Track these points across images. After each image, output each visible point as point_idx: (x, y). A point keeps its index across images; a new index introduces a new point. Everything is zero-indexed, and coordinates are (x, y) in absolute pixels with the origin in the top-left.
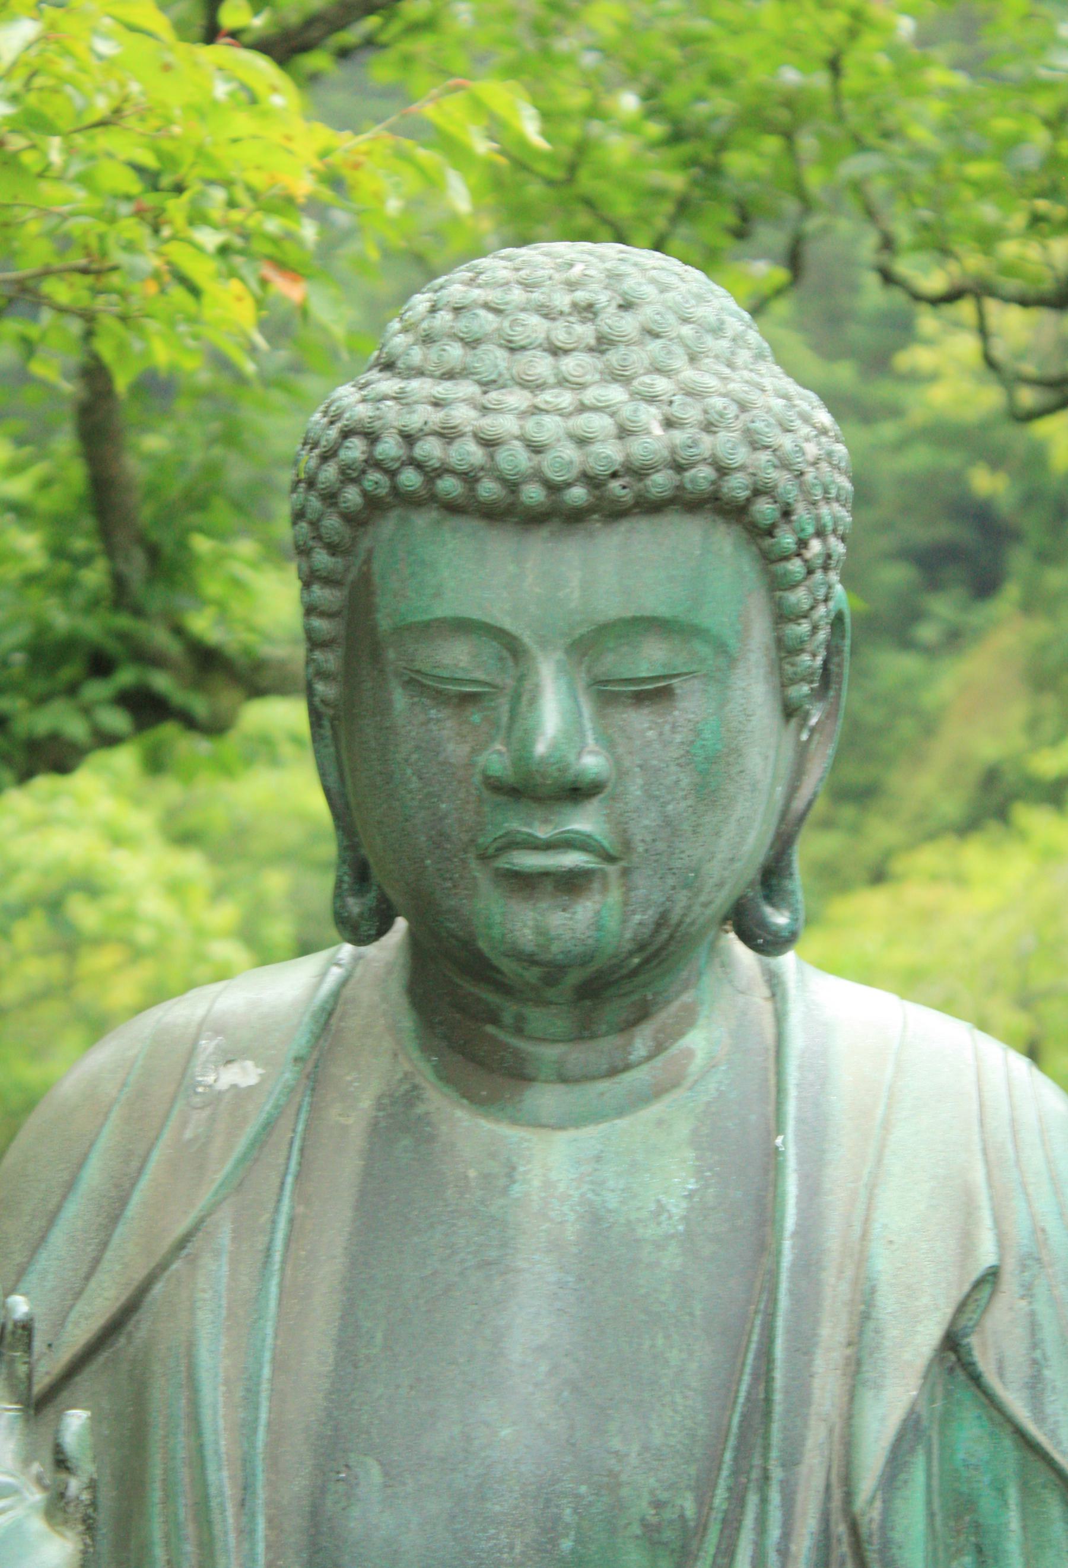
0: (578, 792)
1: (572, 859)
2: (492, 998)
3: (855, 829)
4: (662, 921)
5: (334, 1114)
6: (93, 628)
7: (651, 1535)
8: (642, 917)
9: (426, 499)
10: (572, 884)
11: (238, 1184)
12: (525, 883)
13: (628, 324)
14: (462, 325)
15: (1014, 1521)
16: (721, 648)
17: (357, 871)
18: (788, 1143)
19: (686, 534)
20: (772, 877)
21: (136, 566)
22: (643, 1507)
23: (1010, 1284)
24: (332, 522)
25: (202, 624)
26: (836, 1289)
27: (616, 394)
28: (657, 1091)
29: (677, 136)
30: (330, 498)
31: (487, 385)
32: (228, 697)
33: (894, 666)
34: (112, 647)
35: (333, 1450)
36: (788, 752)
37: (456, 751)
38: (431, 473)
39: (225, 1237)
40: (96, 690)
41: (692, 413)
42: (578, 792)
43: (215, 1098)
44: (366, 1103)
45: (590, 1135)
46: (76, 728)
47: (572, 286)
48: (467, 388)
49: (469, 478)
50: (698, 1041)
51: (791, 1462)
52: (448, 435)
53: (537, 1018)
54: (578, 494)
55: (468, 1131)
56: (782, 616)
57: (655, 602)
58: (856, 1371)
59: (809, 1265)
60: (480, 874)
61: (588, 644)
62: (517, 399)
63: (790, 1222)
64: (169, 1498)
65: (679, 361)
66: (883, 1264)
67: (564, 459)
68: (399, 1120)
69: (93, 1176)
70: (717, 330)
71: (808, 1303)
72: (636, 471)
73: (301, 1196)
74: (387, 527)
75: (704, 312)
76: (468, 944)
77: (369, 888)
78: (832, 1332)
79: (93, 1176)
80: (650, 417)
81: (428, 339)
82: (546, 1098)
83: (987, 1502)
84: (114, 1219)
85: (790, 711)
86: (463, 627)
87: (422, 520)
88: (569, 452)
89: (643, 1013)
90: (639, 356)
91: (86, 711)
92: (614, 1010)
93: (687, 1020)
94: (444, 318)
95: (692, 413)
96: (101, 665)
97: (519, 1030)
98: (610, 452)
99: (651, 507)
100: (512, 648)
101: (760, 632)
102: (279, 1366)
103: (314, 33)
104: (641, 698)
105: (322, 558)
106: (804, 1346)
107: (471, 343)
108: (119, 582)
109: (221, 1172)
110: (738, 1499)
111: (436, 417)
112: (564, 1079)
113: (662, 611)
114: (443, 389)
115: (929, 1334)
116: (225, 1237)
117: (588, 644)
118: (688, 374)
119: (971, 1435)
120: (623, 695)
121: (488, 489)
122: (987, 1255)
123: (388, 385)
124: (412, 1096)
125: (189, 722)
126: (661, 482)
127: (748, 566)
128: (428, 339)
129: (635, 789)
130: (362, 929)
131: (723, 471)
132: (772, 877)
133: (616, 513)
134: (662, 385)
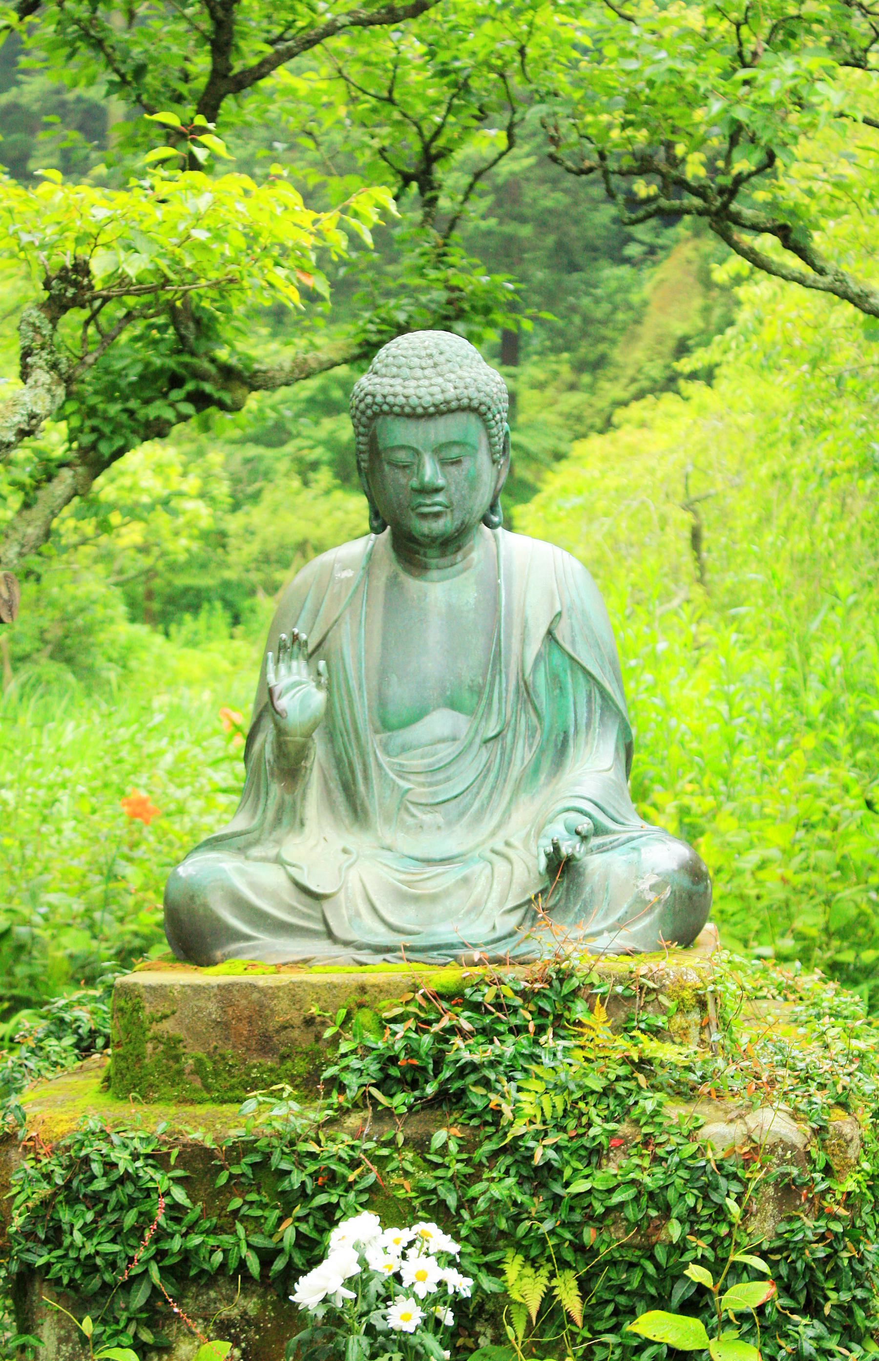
0: (437, 490)
1: (437, 509)
2: (416, 547)
3: (592, 389)
4: (463, 523)
5: (375, 583)
6: (171, 363)
7: (471, 688)
8: (457, 523)
9: (390, 413)
10: (437, 515)
11: (350, 604)
12: (424, 516)
13: (442, 359)
14: (396, 362)
15: (569, 679)
16: (474, 448)
17: (375, 514)
18: (501, 581)
19: (462, 417)
20: (493, 508)
21: (190, 331)
22: (468, 682)
23: (565, 615)
24: (364, 420)
25: (223, 354)
26: (517, 620)
27: (440, 380)
28: (465, 570)
29: (444, 73)
30: (363, 413)
31: (405, 380)
32: (240, 392)
33: (612, 274)
34: (181, 371)
35: (383, 673)
36: (495, 473)
37: (403, 481)
38: (392, 406)
39: (347, 618)
40: (176, 394)
41: (461, 384)
42: (437, 490)
43: (341, 581)
44: (384, 579)
45: (446, 584)
46: (169, 414)
47: (426, 348)
48: (399, 381)
49: (402, 407)
50: (475, 555)
51: (507, 666)
52: (395, 395)
53: (430, 552)
54: (432, 410)
55: (412, 584)
56: (490, 437)
57: (455, 437)
58: (523, 641)
59: (509, 614)
60: (412, 514)
61: (438, 450)
62: (413, 383)
63: (503, 603)
64: (339, 689)
65: (457, 369)
66: (529, 612)
67: (427, 400)
68: (393, 582)
69: (309, 604)
70: (467, 357)
71: (509, 625)
72: (447, 402)
73: (368, 606)
74: (380, 420)
75: (463, 352)
76: (410, 533)
77: (379, 519)
78: (516, 632)
79: (309, 604)
80: (450, 386)
81: (387, 366)
82: (434, 574)
83: (562, 675)
84: (316, 616)
85: (494, 462)
86: (403, 447)
87: (389, 419)
88: (428, 398)
89: (459, 548)
90: (446, 368)
91: (172, 405)
92: (451, 548)
93: (471, 549)
94: (390, 359)
95: (461, 384)
96: (176, 381)
97: (425, 555)
98: (439, 398)
99: (451, 411)
100: (416, 452)
101: (484, 441)
102: (366, 652)
103: (264, 70)
104: (452, 463)
105: (361, 429)
106: (509, 637)
107: (399, 367)
108: (182, 338)
109: (345, 600)
110: (493, 677)
111: (391, 390)
112: (439, 568)
113: (457, 439)
114: (392, 381)
115: (543, 630)
116: (347, 618)
117: (438, 450)
118: (460, 372)
119: (557, 658)
120: (446, 463)
121: (407, 410)
122: (558, 608)
123: (377, 380)
124: (396, 576)
125: (222, 406)
126: (454, 405)
127: (480, 424)
128: (387, 366)
129: (453, 488)
130: (377, 530)
131: (471, 400)
132: (493, 508)
133: (442, 413)
134: (452, 376)
